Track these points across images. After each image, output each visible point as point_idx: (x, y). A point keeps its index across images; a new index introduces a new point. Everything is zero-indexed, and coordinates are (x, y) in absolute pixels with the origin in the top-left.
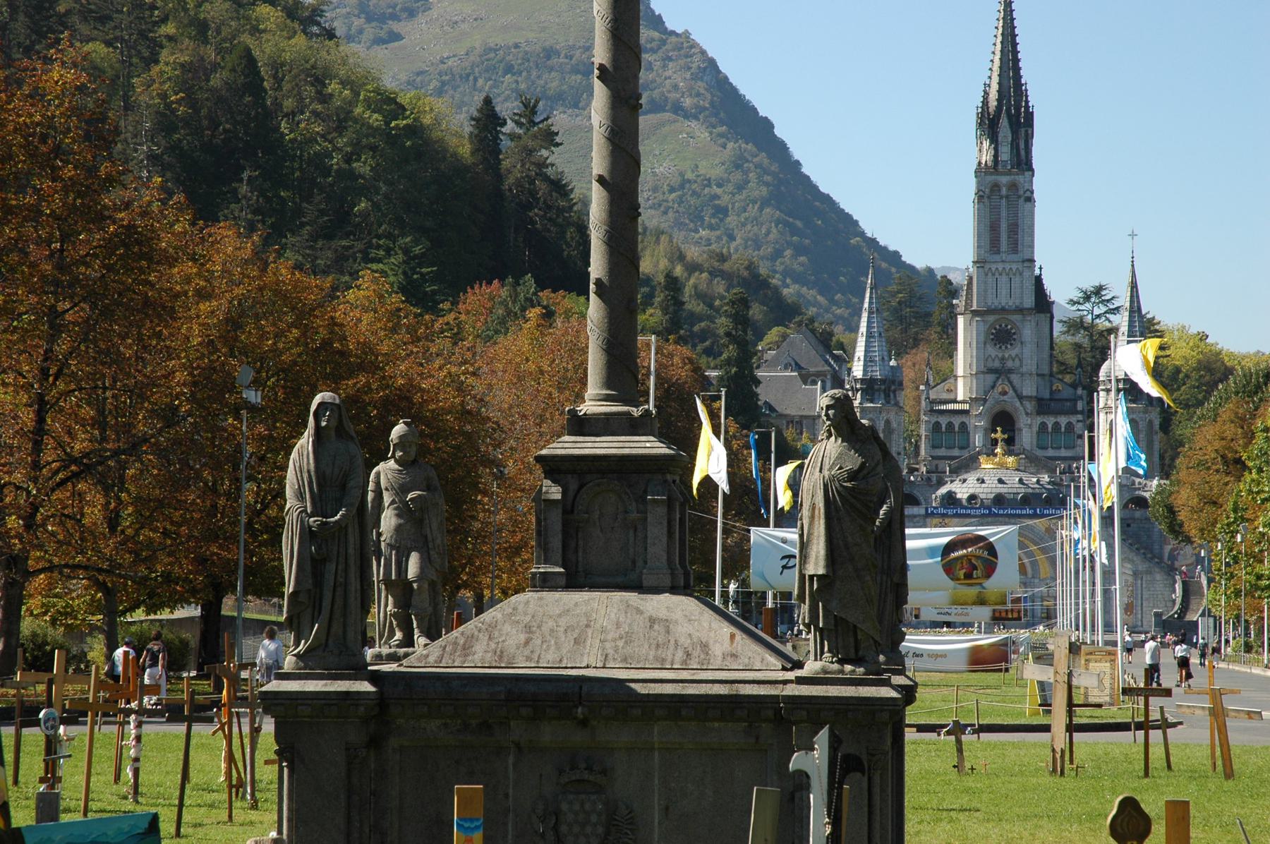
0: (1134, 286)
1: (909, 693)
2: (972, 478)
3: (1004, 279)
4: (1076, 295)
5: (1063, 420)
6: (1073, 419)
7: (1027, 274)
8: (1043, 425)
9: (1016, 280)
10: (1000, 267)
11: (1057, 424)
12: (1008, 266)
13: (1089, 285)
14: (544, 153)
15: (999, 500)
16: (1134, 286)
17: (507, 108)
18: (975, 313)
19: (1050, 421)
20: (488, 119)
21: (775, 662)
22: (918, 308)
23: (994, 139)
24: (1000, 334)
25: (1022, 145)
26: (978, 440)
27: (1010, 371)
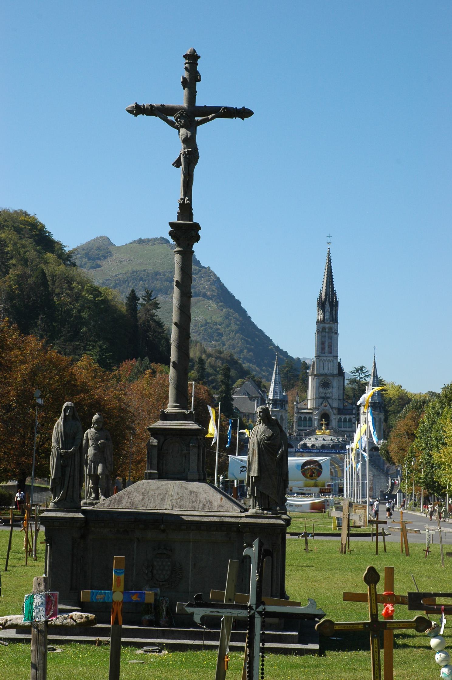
0: (375, 367)
1: (288, 522)
2: (313, 438)
3: (326, 363)
4: (353, 370)
5: (348, 417)
6: (351, 416)
7: (335, 361)
8: (340, 419)
9: (331, 364)
10: (325, 358)
11: (345, 418)
12: (328, 358)
13: (358, 366)
14: (154, 311)
15: (323, 447)
16: (375, 367)
17: (140, 294)
18: (315, 376)
19: (343, 417)
20: (133, 298)
21: (237, 508)
22: (294, 373)
23: (324, 311)
24: (324, 383)
25: (334, 313)
26: (315, 424)
27: (328, 398)
